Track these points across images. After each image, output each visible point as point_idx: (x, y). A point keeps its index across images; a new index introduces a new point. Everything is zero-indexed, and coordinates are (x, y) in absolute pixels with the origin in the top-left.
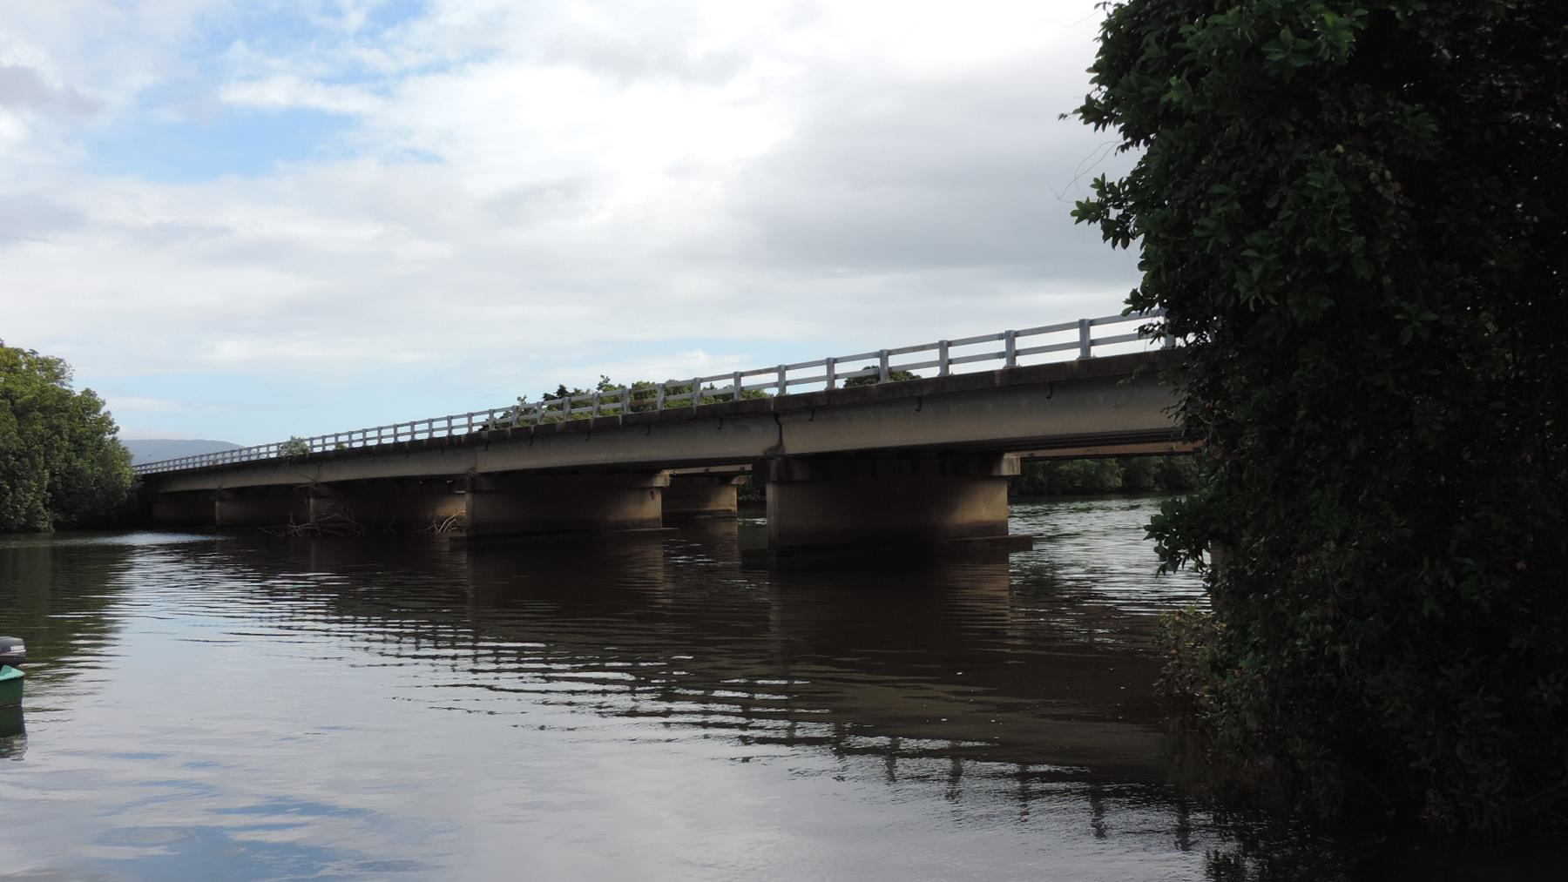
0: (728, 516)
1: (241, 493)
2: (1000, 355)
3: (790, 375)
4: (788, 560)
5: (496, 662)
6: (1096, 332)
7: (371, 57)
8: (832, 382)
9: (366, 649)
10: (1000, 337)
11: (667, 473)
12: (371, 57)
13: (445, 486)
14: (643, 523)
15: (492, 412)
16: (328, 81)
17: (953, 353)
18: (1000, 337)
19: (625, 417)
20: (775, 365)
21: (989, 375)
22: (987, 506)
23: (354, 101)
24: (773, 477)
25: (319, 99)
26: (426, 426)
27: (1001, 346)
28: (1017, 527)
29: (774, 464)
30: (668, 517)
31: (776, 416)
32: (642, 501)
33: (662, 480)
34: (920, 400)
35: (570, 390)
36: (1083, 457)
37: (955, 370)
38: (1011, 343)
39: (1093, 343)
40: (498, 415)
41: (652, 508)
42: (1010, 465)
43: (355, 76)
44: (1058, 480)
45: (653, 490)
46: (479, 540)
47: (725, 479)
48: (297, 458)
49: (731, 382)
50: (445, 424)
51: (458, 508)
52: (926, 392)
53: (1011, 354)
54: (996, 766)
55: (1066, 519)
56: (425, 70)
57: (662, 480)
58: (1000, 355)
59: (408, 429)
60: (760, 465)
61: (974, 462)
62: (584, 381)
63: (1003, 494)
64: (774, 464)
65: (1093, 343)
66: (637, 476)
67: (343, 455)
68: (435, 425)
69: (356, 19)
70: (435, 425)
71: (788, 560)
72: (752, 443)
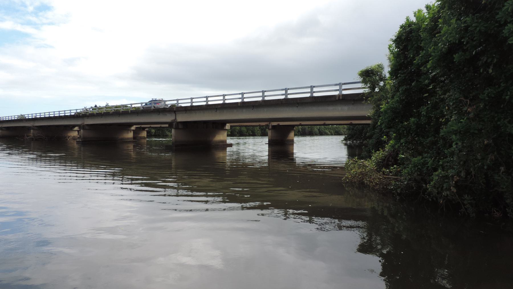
0: (144, 138)
1: (8, 128)
2: (205, 101)
3: (266, 94)
4: (177, 148)
5: (105, 177)
6: (209, 99)
7: (33, 19)
8: (263, 98)
9: (114, 183)
10: (205, 97)
11: (135, 126)
12: (33, 19)
13: (71, 128)
14: (128, 139)
15: (77, 110)
16: (22, 24)
17: (226, 97)
18: (205, 97)
19: (131, 111)
20: (338, 83)
21: (237, 103)
22: (222, 136)
23: (28, 30)
24: (174, 126)
25: (19, 28)
26: (63, 112)
27: (240, 96)
28: (229, 141)
29: (174, 124)
30: (134, 138)
31: (175, 112)
32: (128, 133)
33: (133, 128)
34: (217, 109)
35: (98, 106)
36: (332, 125)
37: (227, 102)
38: (243, 96)
39: (265, 96)
40: (143, 104)
41: (130, 135)
42: (228, 126)
43: (29, 23)
44: (244, 130)
45: (131, 130)
46: (84, 142)
47: (144, 129)
48: (22, 119)
49: (175, 102)
50: (261, 94)
51: (74, 134)
52: (219, 107)
53: (243, 98)
54: (252, 204)
55: (241, 140)
56: (49, 24)
57: (133, 128)
58: (205, 101)
59: (69, 112)
60: (171, 124)
61: (220, 125)
62: (102, 104)
63: (226, 134)
64: (174, 124)
65: (265, 96)
66: (127, 126)
67: (35, 119)
68: (55, 113)
69: (31, 9)
70: (55, 113)
71: (177, 148)
72: (169, 118)
